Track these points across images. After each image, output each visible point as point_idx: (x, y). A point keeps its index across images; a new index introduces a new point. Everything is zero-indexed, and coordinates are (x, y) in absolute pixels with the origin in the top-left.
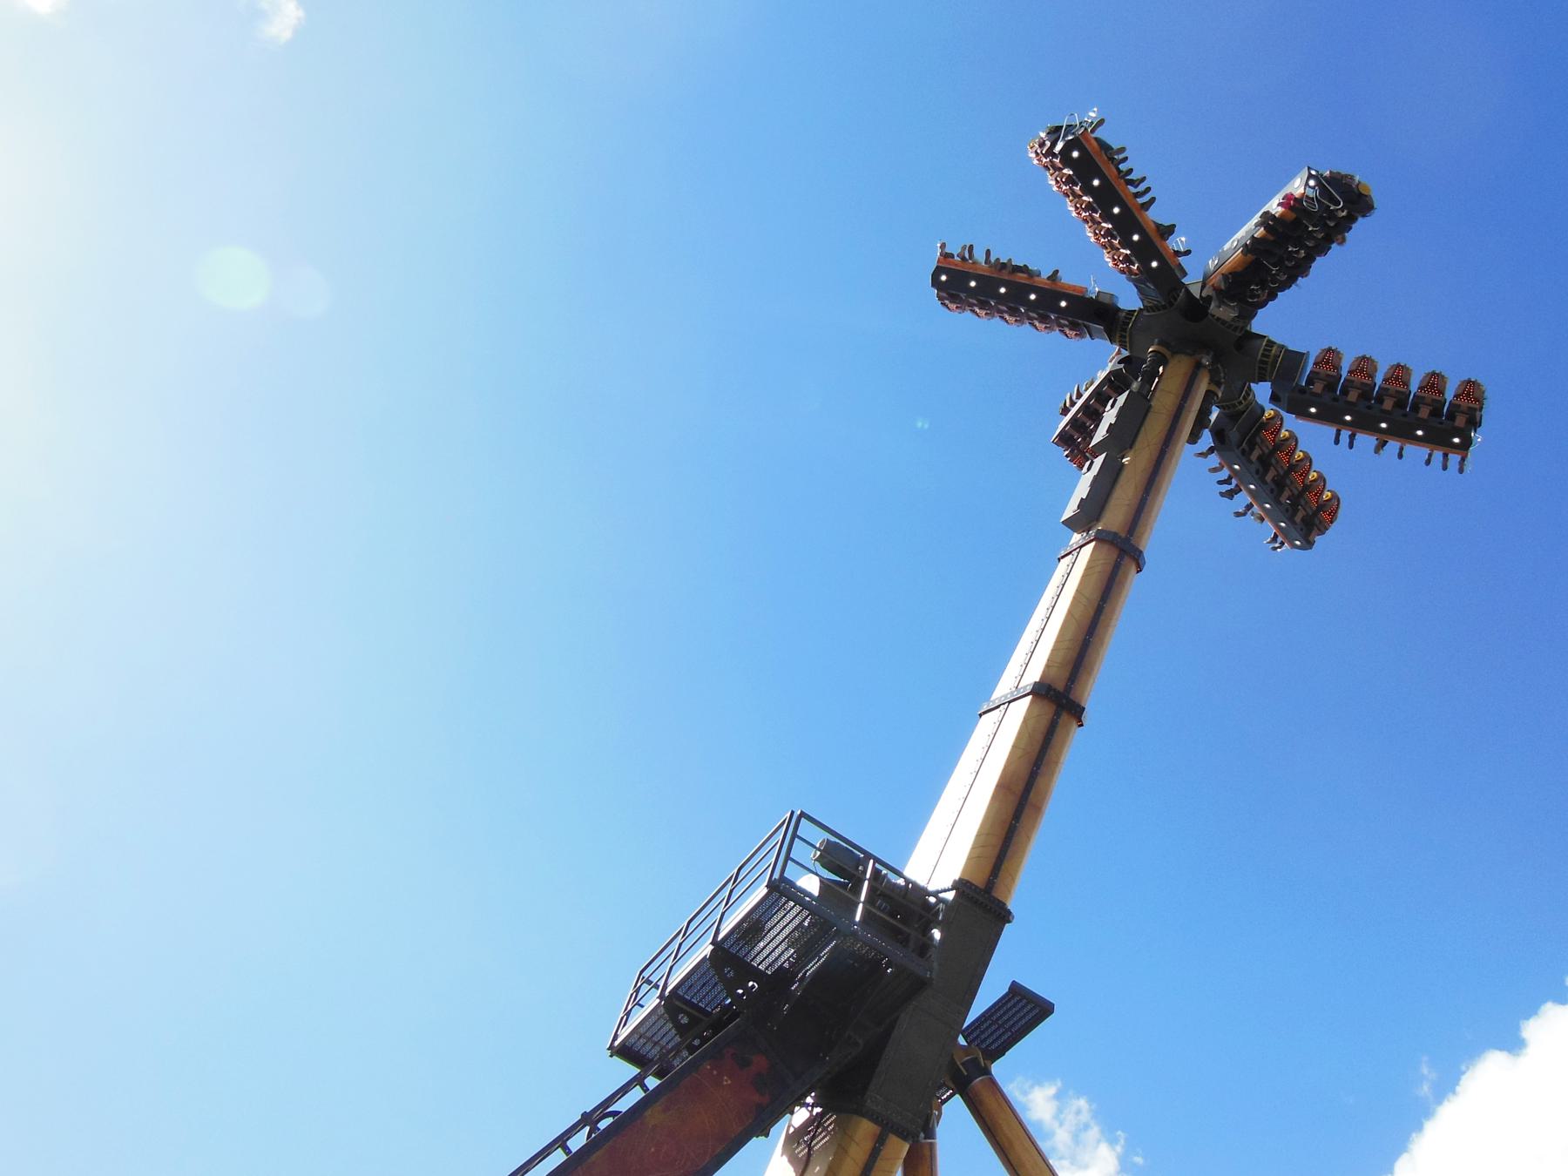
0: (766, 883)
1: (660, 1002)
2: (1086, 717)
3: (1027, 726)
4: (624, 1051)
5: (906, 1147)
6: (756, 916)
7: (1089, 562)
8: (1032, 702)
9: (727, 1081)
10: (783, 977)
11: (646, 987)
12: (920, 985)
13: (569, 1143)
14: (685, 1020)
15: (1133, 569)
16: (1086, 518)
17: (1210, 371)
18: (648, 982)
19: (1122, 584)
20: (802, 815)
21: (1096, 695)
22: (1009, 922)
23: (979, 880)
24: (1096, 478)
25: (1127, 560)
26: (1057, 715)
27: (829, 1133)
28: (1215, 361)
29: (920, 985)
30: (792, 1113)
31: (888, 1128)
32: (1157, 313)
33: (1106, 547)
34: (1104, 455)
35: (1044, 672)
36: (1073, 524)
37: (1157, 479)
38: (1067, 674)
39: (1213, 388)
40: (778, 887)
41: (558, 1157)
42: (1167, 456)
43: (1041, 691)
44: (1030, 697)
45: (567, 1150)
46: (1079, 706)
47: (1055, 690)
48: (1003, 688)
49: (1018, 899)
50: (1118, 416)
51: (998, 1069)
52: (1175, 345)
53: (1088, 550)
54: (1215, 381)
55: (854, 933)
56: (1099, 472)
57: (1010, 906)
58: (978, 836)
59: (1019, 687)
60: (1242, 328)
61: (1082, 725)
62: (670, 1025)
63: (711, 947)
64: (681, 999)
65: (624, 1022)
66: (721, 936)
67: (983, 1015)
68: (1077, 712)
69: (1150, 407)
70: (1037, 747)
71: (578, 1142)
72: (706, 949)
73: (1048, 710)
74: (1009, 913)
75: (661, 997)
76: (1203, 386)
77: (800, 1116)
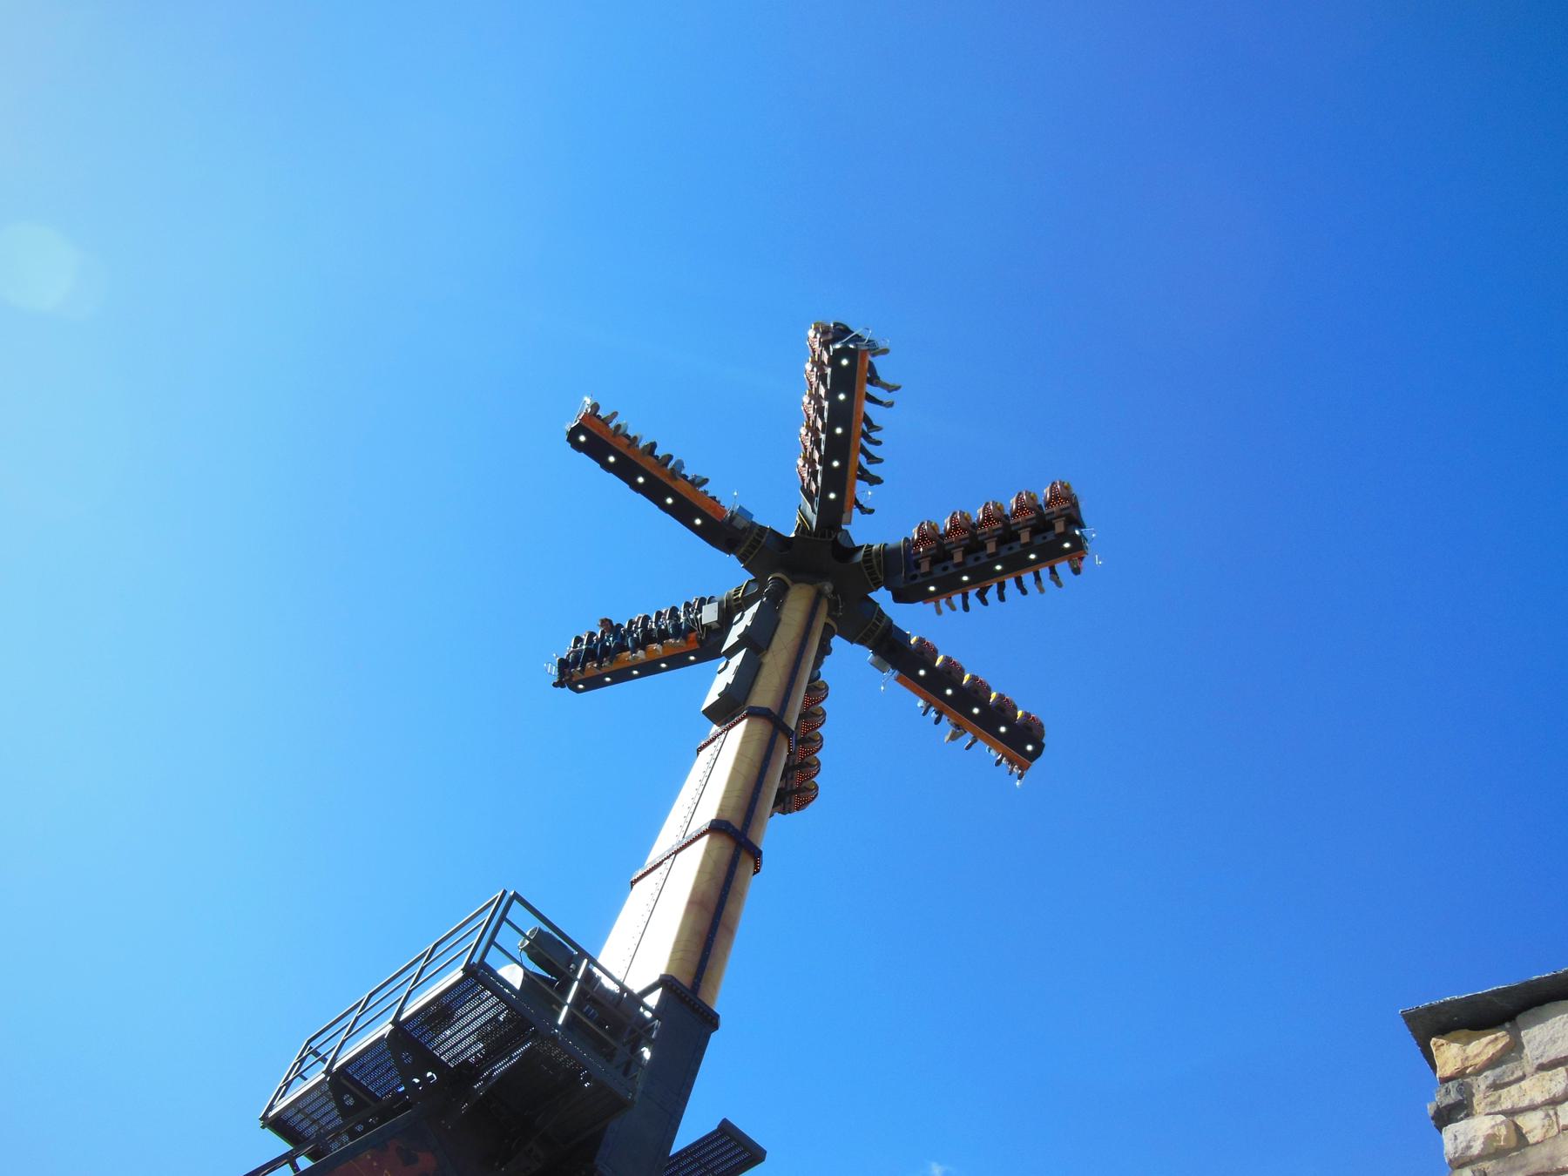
0: (462, 966)
1: (325, 1078)
6: (445, 1001)
10: (466, 1072)
11: (311, 1059)
18: (316, 1053)
20: (516, 896)
40: (476, 973)
47: (733, 827)
49: (723, 1001)
51: (836, 636)
57: (717, 1008)
62: (332, 1104)
64: (350, 1078)
66: (403, 1017)
67: (685, 1150)
72: (385, 1028)
74: (716, 1017)
75: (328, 1072)
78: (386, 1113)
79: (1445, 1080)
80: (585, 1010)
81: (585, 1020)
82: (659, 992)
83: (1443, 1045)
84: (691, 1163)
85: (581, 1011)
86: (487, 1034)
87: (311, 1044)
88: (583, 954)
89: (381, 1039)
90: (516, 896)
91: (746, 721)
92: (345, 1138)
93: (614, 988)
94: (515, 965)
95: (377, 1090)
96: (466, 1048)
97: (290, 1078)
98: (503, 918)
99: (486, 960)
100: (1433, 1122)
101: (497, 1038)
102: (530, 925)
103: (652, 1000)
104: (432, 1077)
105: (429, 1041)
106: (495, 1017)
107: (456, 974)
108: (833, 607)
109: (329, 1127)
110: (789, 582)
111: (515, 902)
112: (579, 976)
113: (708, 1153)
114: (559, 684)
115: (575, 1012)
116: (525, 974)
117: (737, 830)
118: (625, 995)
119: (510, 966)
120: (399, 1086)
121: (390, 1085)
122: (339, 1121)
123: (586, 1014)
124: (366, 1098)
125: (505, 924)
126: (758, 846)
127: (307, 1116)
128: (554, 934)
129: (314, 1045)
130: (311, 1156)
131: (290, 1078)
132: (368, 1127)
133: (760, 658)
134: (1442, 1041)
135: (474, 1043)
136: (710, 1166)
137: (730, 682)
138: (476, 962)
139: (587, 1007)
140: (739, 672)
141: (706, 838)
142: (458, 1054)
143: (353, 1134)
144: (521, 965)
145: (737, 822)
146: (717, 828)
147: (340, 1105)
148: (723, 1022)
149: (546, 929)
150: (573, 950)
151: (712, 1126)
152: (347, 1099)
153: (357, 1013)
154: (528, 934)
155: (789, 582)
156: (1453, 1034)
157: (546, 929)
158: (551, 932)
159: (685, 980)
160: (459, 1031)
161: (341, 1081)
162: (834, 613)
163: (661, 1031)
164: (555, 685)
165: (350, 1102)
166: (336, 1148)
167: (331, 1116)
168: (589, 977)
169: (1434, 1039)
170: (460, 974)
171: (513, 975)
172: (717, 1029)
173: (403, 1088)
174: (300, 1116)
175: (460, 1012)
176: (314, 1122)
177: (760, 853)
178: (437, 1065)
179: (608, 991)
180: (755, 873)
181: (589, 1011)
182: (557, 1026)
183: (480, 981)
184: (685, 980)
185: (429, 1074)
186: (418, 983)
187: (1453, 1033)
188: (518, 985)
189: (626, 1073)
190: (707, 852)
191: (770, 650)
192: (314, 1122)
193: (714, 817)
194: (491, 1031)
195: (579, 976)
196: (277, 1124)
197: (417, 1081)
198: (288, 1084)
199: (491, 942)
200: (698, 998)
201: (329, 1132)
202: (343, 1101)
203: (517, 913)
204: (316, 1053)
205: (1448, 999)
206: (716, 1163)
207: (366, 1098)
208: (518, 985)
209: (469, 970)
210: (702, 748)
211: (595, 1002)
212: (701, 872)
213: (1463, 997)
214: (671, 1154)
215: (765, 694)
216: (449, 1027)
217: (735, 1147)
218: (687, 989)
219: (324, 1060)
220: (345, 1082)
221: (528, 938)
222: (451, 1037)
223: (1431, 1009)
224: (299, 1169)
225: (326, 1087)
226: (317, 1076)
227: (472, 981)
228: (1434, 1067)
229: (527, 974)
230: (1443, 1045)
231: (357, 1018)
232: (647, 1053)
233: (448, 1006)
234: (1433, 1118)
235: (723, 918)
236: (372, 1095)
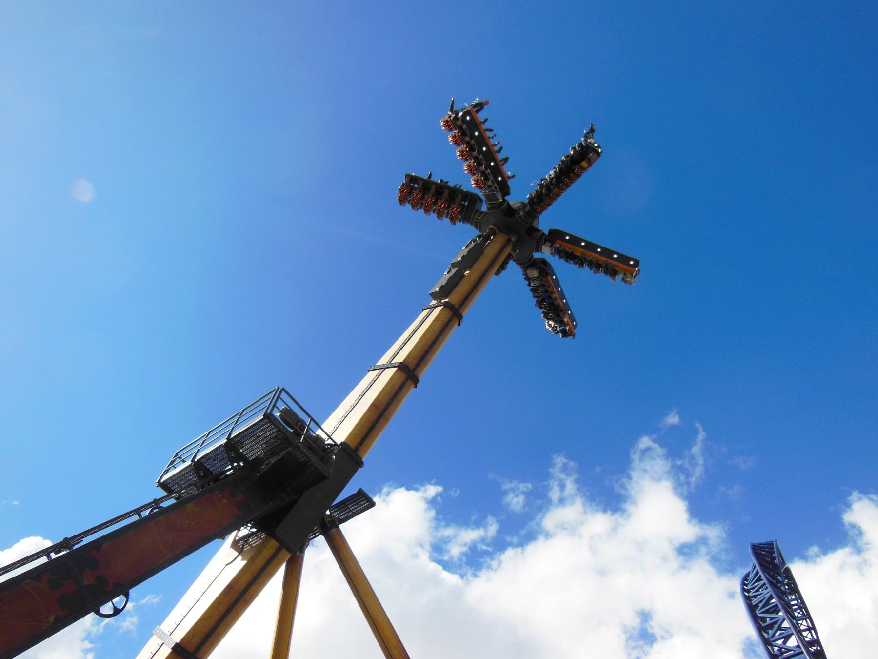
0: (191, 460)
1: (192, 464)
2: (419, 384)
3: (392, 381)
4: (164, 485)
5: (290, 556)
6: (239, 438)
7: (438, 315)
8: (397, 371)
9: (225, 501)
10: (258, 461)
11: (178, 460)
12: (323, 478)
13: (141, 513)
14: (202, 474)
15: (413, 387)
16: (445, 291)
17: (513, 244)
18: (180, 458)
19: (450, 329)
20: (283, 389)
21: (424, 375)
22: (361, 467)
23: (353, 445)
24: (451, 277)
25: (409, 382)
26: (407, 379)
27: (261, 539)
28: (518, 240)
29: (323, 478)
30: (239, 530)
31: (283, 545)
32: (492, 211)
33: (448, 310)
34: (458, 268)
35: (405, 359)
36: (434, 296)
37: (478, 286)
38: (416, 363)
39: (512, 253)
41: (136, 518)
42: (485, 277)
43: (402, 367)
44: (397, 368)
45: (139, 515)
46: (417, 378)
47: (409, 368)
48: (383, 361)
49: (367, 458)
50: (468, 252)
52: (501, 228)
53: (438, 310)
54: (514, 250)
55: (299, 447)
56: (453, 275)
57: (364, 460)
58: (357, 425)
59: (392, 362)
60: (530, 223)
61: (416, 387)
62: (195, 474)
63: (226, 441)
64: (202, 464)
65: (166, 472)
66: (232, 436)
67: (342, 502)
68: (416, 381)
69: (483, 253)
70: (394, 392)
71: (146, 513)
72: (224, 441)
73: (403, 376)
74: (363, 463)
75: (193, 461)
76: (508, 250)
77: (244, 532)
89: (222, 445)
90: (283, 389)
101: (275, 446)
111: (283, 392)
114: (574, 336)
125: (279, 400)
146: (402, 367)
147: (198, 475)
161: (198, 466)
164: (574, 338)
182: (300, 443)
227: (267, 420)
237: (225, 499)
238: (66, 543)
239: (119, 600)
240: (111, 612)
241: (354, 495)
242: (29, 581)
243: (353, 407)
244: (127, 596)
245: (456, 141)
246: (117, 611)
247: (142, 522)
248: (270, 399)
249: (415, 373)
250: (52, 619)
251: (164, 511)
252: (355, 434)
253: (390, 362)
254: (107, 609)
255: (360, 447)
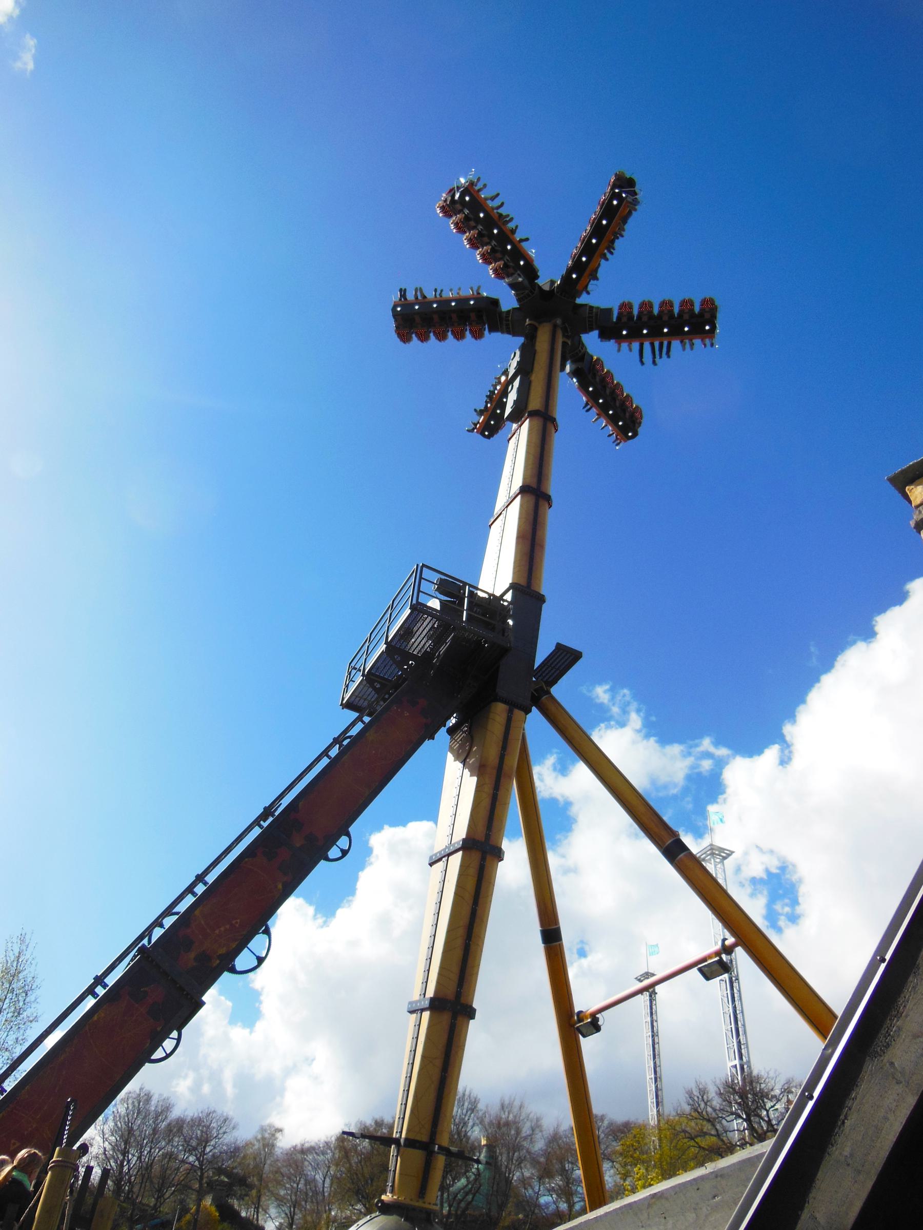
0: (409, 607)
1: (363, 678)
8: (522, 497)
10: (427, 657)
11: (354, 672)
12: (504, 651)
18: (355, 669)
20: (423, 565)
21: (554, 488)
26: (454, 1018)
41: (325, 761)
43: (468, 845)
47: (532, 487)
49: (546, 587)
57: (543, 591)
59: (452, 843)
62: (371, 689)
63: (385, 646)
64: (373, 675)
67: (543, 663)
71: (334, 752)
72: (383, 647)
75: (363, 675)
78: (396, 686)
79: (917, 507)
80: (474, 610)
81: (476, 615)
82: (511, 592)
83: (913, 489)
84: (547, 668)
85: (473, 612)
86: (431, 635)
87: (351, 665)
88: (465, 584)
90: (423, 565)
91: (528, 420)
92: (382, 703)
93: (486, 596)
94: (434, 599)
95: (389, 677)
96: (424, 645)
97: (347, 683)
98: (421, 578)
99: (419, 601)
100: (915, 530)
101: (440, 632)
102: (435, 577)
103: (509, 597)
104: (412, 663)
105: (405, 647)
106: (433, 627)
107: (407, 612)
108: (565, 331)
109: (373, 699)
110: (537, 324)
112: (466, 595)
113: (555, 661)
115: (470, 613)
116: (440, 602)
117: (534, 488)
118: (492, 597)
119: (431, 600)
120: (398, 672)
121: (392, 673)
122: (376, 696)
123: (475, 612)
124: (384, 682)
126: (548, 493)
127: (361, 698)
128: (448, 579)
129: (353, 665)
130: (369, 715)
131: (347, 683)
132: (390, 695)
133: (529, 378)
134: (912, 487)
135: (427, 641)
136: (554, 670)
137: (515, 399)
138: (415, 603)
139: (475, 609)
140: (519, 391)
141: (519, 497)
142: (421, 649)
143: (385, 700)
144: (437, 598)
145: (534, 485)
146: (524, 490)
147: (374, 689)
148: (547, 598)
149: (443, 577)
150: (459, 583)
151: (552, 648)
152: (376, 685)
153: (367, 644)
154: (435, 582)
155: (537, 324)
156: (917, 481)
157: (443, 577)
158: (446, 578)
159: (523, 582)
160: (418, 638)
161: (370, 677)
162: (566, 334)
163: (514, 609)
165: (378, 686)
166: (379, 709)
167: (372, 695)
168: (472, 595)
169: (907, 488)
170: (409, 611)
171: (435, 604)
172: (545, 602)
173: (400, 672)
174: (358, 699)
175: (415, 629)
176: (365, 699)
177: (550, 497)
178: (414, 657)
179: (483, 598)
180: (550, 508)
181: (477, 610)
183: (420, 612)
184: (523, 582)
185: (410, 662)
186: (391, 622)
187: (917, 481)
188: (439, 608)
189: (503, 635)
190: (521, 506)
191: (534, 372)
192: (365, 699)
193: (521, 485)
194: (433, 633)
195: (466, 595)
196: (349, 705)
197: (406, 667)
198: (347, 686)
199: (419, 591)
200: (532, 590)
201: (374, 702)
202: (375, 687)
203: (427, 573)
204: (355, 669)
205: (911, 463)
206: (559, 665)
207: (384, 682)
208: (439, 608)
209: (413, 608)
210: (510, 439)
211: (478, 605)
212: (520, 518)
213: (919, 460)
214: (536, 666)
215: (535, 403)
216: (413, 638)
217: (566, 655)
218: (523, 586)
219: (360, 670)
220: (372, 677)
221: (436, 584)
222: (415, 642)
223: (902, 472)
224: (331, 757)
225: (365, 682)
226: (358, 679)
228: (910, 502)
229: (441, 601)
230: (913, 489)
231: (368, 647)
232: (511, 622)
233: (409, 628)
234: (914, 528)
235: (536, 540)
236: (387, 680)
237: (405, 712)
238: (267, 812)
239: (343, 842)
240: (340, 854)
241: (551, 654)
242: (246, 860)
243: (440, 893)
244: (348, 835)
245: (486, 259)
246: (345, 853)
247: (334, 762)
248: (412, 584)
249: (490, 843)
250: (280, 886)
251: (355, 740)
252: (518, 571)
253: (509, 498)
254: (334, 852)
255: (477, 908)
